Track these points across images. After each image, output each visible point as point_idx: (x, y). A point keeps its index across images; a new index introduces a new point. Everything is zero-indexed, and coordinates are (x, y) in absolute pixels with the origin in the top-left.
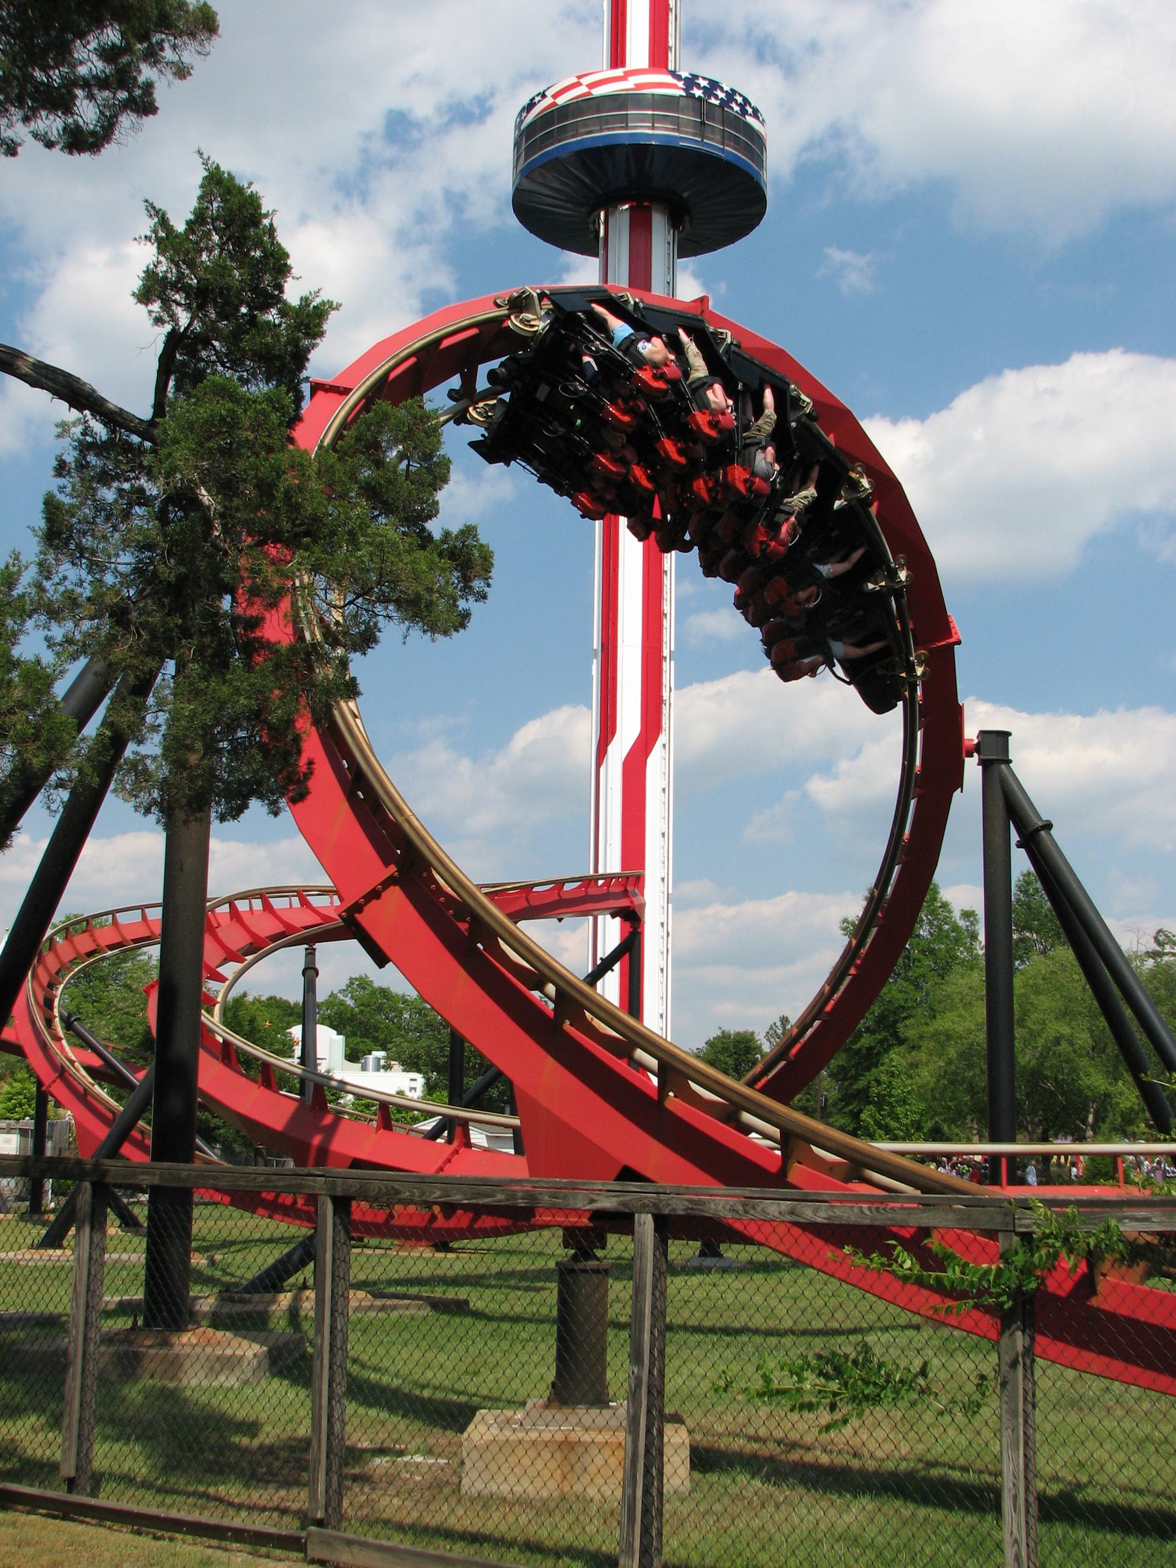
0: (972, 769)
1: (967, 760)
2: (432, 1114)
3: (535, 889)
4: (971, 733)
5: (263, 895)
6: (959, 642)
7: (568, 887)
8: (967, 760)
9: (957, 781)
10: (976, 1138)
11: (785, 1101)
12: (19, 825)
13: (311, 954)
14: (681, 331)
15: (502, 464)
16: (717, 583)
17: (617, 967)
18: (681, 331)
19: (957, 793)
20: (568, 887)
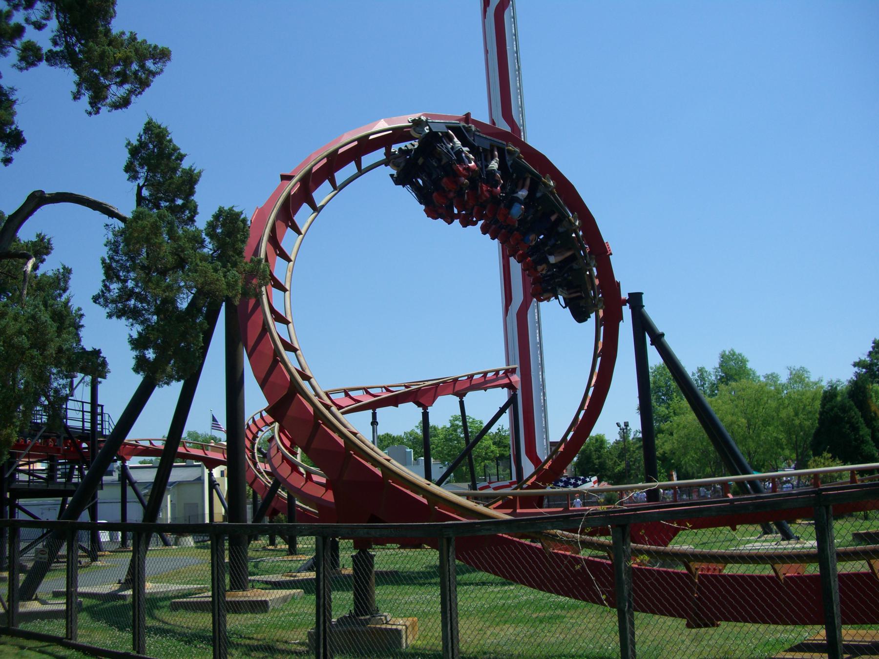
0: (627, 311)
1: (624, 307)
2: (529, 487)
3: (460, 379)
4: (624, 295)
5: (346, 392)
6: (611, 254)
7: (476, 377)
8: (624, 307)
9: (620, 318)
10: (821, 476)
11: (806, 467)
12: (605, 242)
13: (374, 415)
14: (224, 304)
15: (401, 186)
16: (172, 384)
17: (507, 411)
18: (224, 304)
19: (621, 323)
20: (476, 377)
